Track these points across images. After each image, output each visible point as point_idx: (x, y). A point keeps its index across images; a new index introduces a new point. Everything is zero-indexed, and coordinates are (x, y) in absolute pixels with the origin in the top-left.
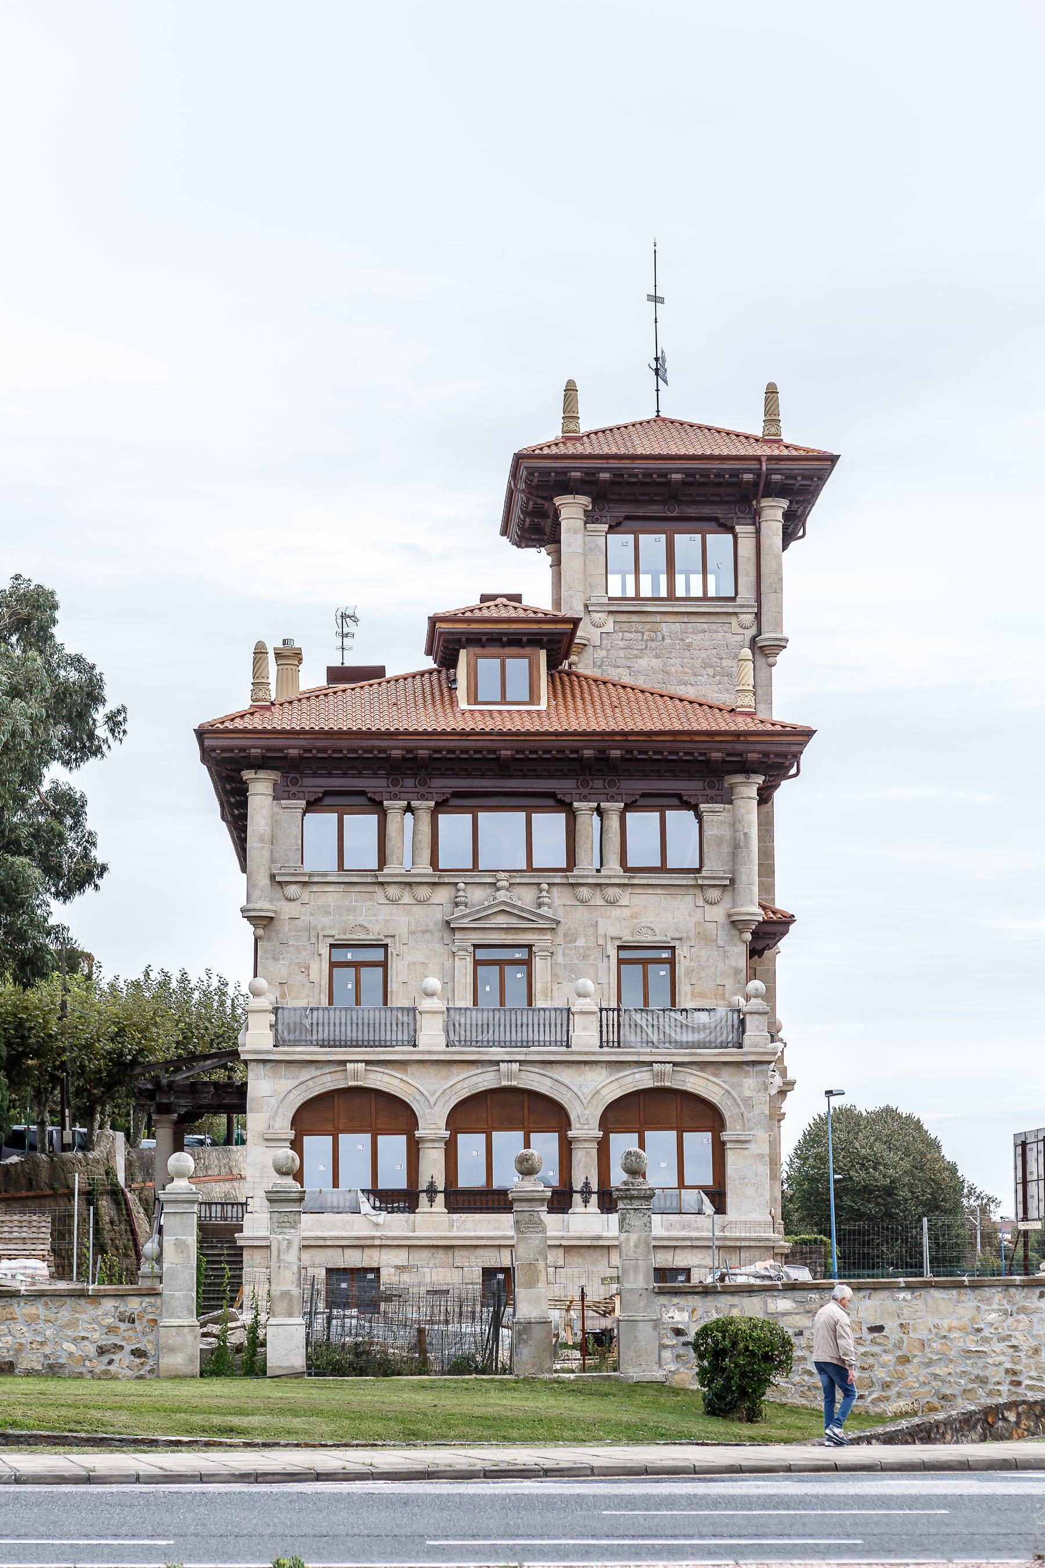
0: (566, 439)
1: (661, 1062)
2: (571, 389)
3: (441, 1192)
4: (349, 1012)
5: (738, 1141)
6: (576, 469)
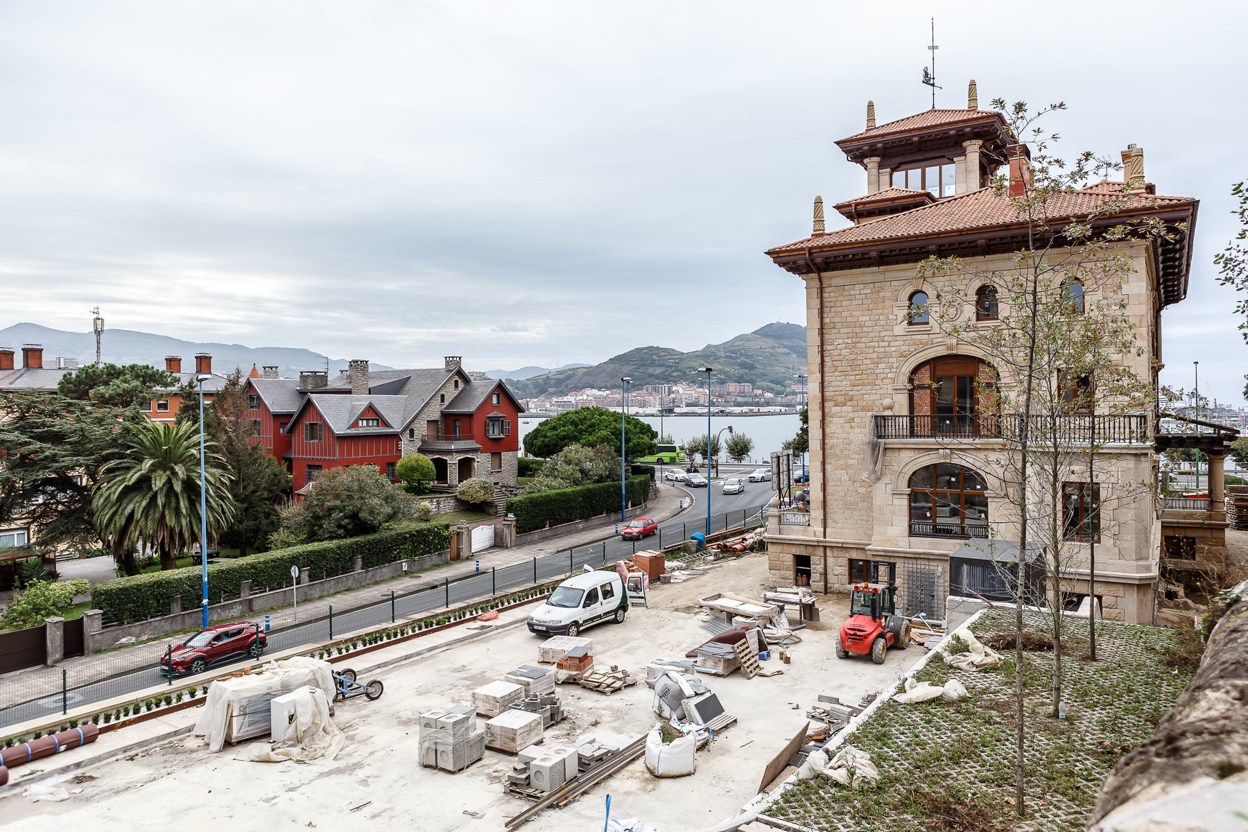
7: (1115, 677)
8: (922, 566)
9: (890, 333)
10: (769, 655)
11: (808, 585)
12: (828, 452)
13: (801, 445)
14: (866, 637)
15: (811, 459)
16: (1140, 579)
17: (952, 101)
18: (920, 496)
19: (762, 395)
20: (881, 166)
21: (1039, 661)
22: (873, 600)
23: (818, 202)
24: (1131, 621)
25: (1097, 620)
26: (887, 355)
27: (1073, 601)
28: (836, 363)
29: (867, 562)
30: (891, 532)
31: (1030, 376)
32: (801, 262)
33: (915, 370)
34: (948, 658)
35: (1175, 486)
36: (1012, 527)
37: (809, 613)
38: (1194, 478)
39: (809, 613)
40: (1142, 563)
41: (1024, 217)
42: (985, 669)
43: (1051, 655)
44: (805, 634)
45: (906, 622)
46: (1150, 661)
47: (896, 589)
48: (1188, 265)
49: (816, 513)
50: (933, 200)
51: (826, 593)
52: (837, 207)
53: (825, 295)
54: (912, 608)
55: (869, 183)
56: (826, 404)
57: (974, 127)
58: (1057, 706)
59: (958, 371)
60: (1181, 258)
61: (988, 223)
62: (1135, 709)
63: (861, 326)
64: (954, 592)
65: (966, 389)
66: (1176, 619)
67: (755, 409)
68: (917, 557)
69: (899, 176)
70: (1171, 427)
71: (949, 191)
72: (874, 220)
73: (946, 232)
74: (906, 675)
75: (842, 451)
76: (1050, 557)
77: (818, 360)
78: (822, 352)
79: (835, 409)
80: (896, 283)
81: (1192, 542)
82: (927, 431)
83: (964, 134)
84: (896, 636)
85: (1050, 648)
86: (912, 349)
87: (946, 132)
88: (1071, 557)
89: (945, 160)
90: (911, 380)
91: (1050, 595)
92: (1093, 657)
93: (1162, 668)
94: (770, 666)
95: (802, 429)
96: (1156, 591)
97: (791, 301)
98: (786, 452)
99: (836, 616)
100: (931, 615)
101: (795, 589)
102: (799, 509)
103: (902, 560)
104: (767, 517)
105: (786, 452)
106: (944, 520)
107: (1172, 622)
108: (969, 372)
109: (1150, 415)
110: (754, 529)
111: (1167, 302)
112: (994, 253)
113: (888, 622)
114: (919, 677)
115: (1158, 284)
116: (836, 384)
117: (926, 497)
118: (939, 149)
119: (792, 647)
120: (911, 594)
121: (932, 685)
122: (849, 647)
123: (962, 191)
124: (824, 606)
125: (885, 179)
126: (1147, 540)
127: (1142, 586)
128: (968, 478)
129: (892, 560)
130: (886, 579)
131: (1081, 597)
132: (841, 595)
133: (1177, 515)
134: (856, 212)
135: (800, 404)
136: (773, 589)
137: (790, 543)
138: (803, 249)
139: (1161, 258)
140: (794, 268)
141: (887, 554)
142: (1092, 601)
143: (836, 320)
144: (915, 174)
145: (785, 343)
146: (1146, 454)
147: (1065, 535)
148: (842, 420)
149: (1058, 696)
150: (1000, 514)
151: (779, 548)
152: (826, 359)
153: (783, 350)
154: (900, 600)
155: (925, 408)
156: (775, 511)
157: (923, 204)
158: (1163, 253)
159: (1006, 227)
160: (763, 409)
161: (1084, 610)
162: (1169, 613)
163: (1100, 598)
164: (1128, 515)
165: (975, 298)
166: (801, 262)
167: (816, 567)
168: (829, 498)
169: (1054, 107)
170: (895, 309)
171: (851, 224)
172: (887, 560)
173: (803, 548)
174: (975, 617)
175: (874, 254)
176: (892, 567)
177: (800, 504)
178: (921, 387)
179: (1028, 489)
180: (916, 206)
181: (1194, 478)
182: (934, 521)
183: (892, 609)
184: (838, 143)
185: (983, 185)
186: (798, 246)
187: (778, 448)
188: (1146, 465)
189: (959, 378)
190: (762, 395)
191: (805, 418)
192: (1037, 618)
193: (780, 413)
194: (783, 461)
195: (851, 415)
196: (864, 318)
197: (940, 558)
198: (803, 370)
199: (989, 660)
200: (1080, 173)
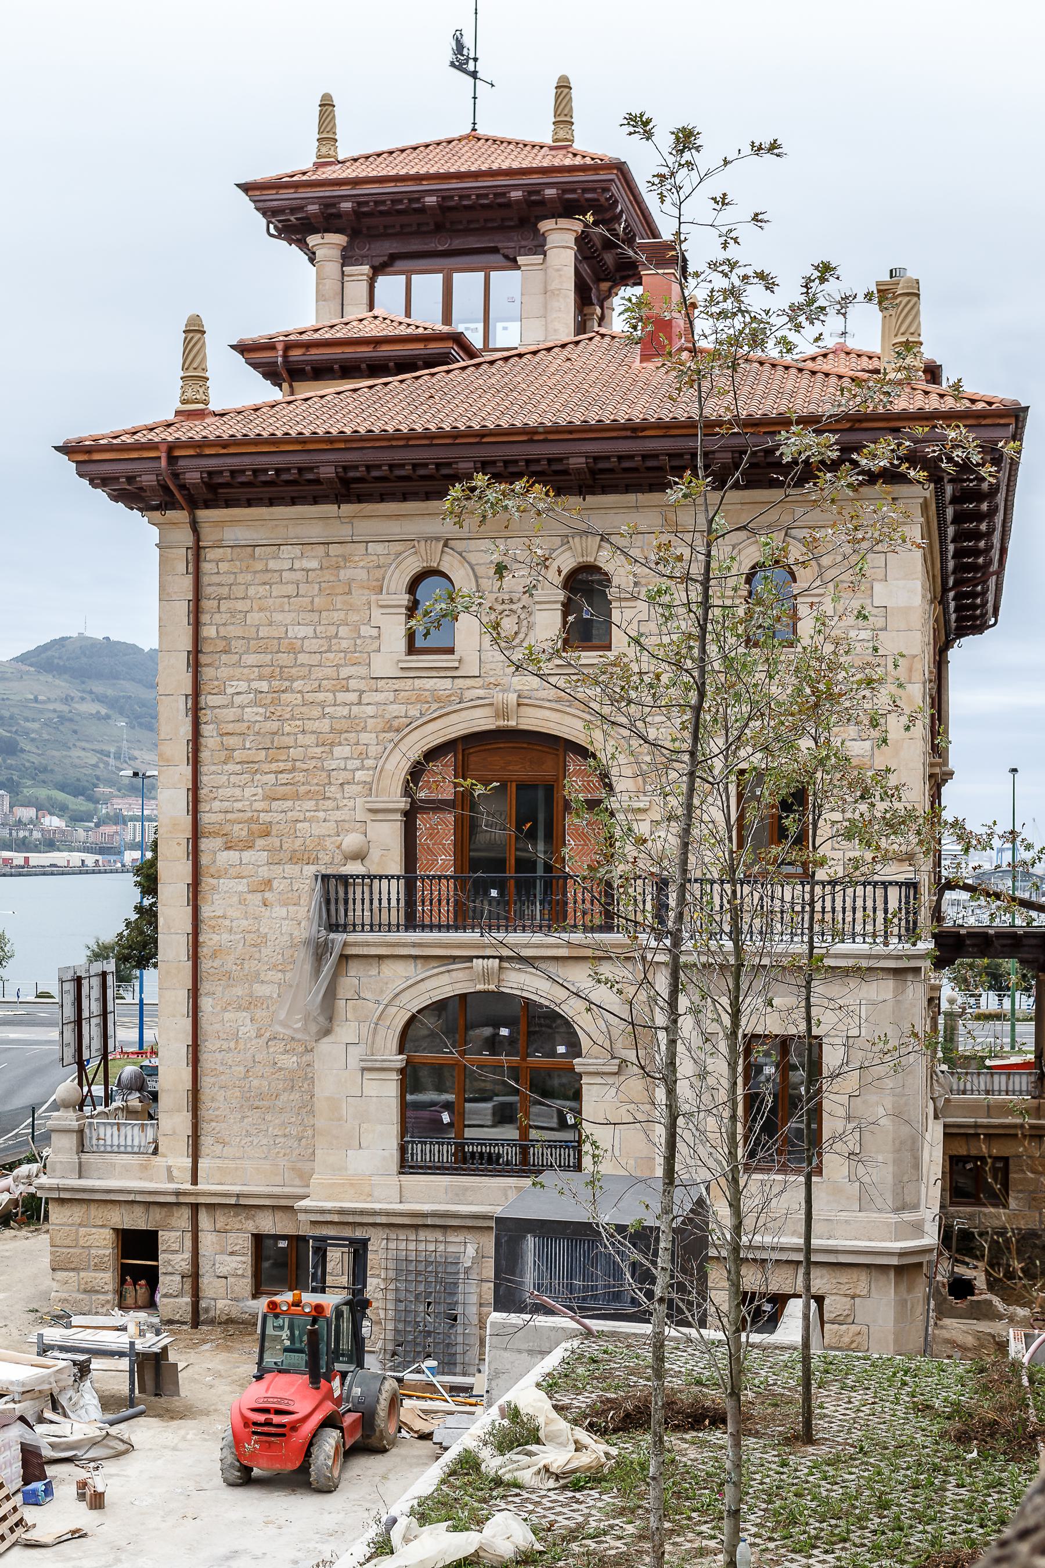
0: (318, 166)
1: (483, 957)
2: (327, 105)
3: (968, 1150)
4: (385, 882)
5: (597, 1074)
6: (516, 187)
7: (852, 1477)
8: (429, 1245)
9: (363, 669)
10: (48, 1491)
11: (151, 1305)
12: (205, 965)
13: (137, 949)
14: (294, 1427)
15: (161, 985)
16: (902, 1254)
17: (516, 122)
18: (424, 1074)
19: (35, 822)
20: (347, 258)
21: (693, 1453)
22: (313, 1335)
23: (194, 331)
24: (881, 1348)
25: (815, 1351)
26: (355, 725)
27: (762, 1311)
28: (231, 741)
29: (298, 1241)
30: (354, 1163)
31: (692, 774)
32: (148, 480)
33: (416, 773)
34: (492, 1463)
35: (964, 1046)
36: (630, 1147)
37: (153, 1374)
38: (1007, 1026)
39: (153, 1374)
40: (908, 1216)
41: (685, 409)
42: (574, 1482)
43: (719, 1437)
44: (143, 1432)
45: (390, 1385)
46: (921, 1433)
47: (367, 1303)
48: (1003, 551)
49: (174, 1119)
50: (470, 352)
51: (196, 1323)
52: (242, 348)
53: (206, 567)
54: (406, 1349)
55: (320, 297)
56: (205, 844)
57: (565, 188)
58: (732, 1553)
59: (521, 770)
60: (989, 533)
61: (593, 418)
62: (893, 1545)
63: (293, 651)
64: (507, 1299)
65: (540, 809)
66: (970, 1341)
67: (18, 858)
68: (417, 1224)
69: (390, 286)
70: (964, 913)
71: (507, 335)
72: (329, 388)
73: (499, 432)
74: (394, 1512)
75: (241, 961)
76: (721, 1210)
77: (186, 730)
78: (196, 711)
79: (226, 857)
80: (380, 548)
81: (1003, 1166)
82: (446, 913)
83: (542, 203)
84: (367, 1419)
85: (718, 1420)
86: (414, 712)
87: (501, 193)
88: (768, 1201)
89: (498, 259)
90: (407, 792)
91: (720, 1297)
92: (807, 1436)
93: (948, 1448)
94: (47, 1520)
95: (139, 909)
96: (931, 1279)
97: (115, 579)
98: (97, 967)
99: (220, 1381)
100: (448, 1365)
101: (118, 1317)
102: (130, 1113)
103: (382, 1233)
104: (46, 1138)
105: (97, 967)
106: (483, 1130)
107: (963, 1348)
108: (543, 772)
109: (925, 880)
110: (12, 1167)
111: (962, 632)
112: (605, 490)
113: (349, 1387)
114: (423, 1515)
115: (945, 590)
116: (231, 794)
117: (440, 1075)
118: (483, 230)
119: (110, 1467)
120: (403, 1316)
121: (455, 1529)
122: (253, 1455)
123: (536, 338)
124: (192, 1357)
125: (357, 289)
126: (917, 1165)
127: (905, 1269)
128: (544, 1025)
129: (359, 1234)
130: (344, 1280)
131: (780, 1300)
132: (234, 1326)
133: (972, 1108)
134: (288, 363)
135: (133, 847)
136: (62, 1319)
137: (107, 1200)
138: (151, 446)
139: (951, 530)
140: (130, 493)
141: (348, 1219)
142: (807, 1306)
143: (232, 631)
144: (428, 285)
145: (99, 688)
146: (917, 970)
147: (752, 1155)
148: (242, 886)
149: (736, 1530)
150: (607, 1107)
151: (76, 1213)
152: (207, 730)
153: (92, 708)
154: (377, 1332)
155: (440, 858)
156: (68, 1118)
157: (443, 359)
158: (957, 519)
159: (633, 430)
160: (37, 859)
161: (790, 1330)
162: (957, 1329)
163: (820, 1300)
164: (878, 1107)
165: (561, 595)
166: (148, 480)
167: (173, 1259)
168: (206, 1082)
169: (757, 149)
170: (376, 612)
171: (272, 393)
172: (347, 1233)
173: (139, 1211)
174: (552, 1361)
175: (327, 472)
176: (359, 1250)
177: (134, 1100)
178: (437, 806)
179: (680, 1048)
180: (431, 362)
181: (1007, 1026)
182: (460, 1135)
183: (357, 1355)
184: (246, 188)
185: (581, 327)
186: (128, 439)
187: (78, 959)
188: (915, 993)
189: (522, 787)
190: (35, 822)
191: (148, 879)
192: (694, 1355)
193: (83, 870)
194: (92, 990)
195: (264, 872)
196: (302, 631)
197: (473, 1225)
198: (146, 761)
199: (584, 1459)
200: (805, 310)
